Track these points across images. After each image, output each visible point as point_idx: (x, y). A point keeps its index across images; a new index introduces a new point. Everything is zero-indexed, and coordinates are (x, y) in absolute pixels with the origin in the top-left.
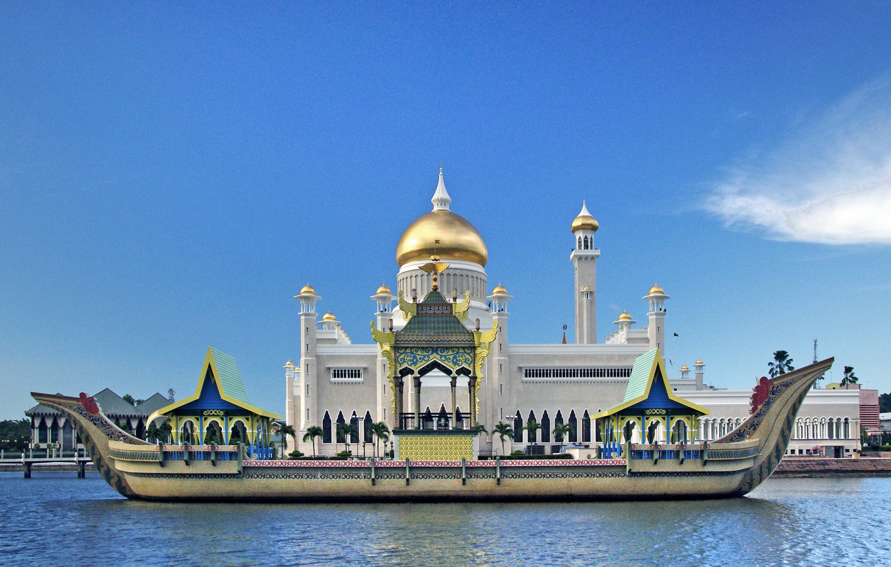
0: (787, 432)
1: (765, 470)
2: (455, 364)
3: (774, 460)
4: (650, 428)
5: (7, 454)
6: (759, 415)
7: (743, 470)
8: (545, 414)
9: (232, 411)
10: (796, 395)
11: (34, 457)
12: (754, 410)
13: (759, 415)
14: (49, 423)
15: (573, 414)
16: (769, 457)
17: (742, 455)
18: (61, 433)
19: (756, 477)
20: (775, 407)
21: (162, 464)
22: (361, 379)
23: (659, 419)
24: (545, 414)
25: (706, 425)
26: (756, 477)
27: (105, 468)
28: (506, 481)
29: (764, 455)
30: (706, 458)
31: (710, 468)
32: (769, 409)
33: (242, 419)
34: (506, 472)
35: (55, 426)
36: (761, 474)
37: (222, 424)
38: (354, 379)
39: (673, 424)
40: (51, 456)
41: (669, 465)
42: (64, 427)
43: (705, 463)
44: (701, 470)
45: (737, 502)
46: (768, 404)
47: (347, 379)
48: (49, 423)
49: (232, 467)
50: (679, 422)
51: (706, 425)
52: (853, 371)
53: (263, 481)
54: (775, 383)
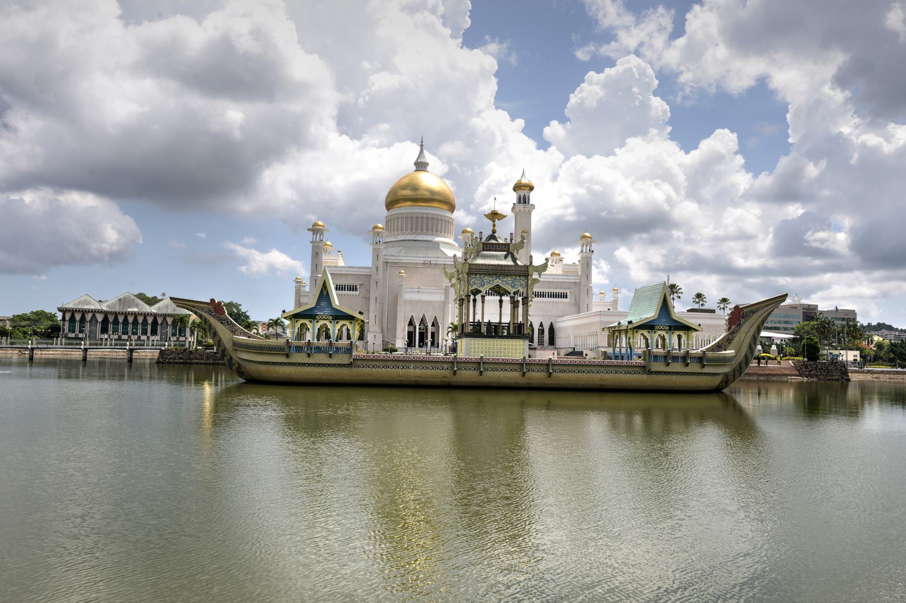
0: (753, 346)
1: (737, 373)
2: (513, 287)
4: (319, 329)
5: (13, 340)
10: (760, 319)
11: (136, 345)
12: (729, 329)
16: (740, 364)
17: (725, 360)
18: (87, 325)
19: (731, 378)
20: (744, 328)
21: (287, 356)
22: (357, 293)
26: (731, 378)
27: (228, 357)
29: (735, 363)
31: (706, 370)
32: (740, 329)
35: (83, 319)
36: (734, 375)
37: (330, 326)
38: (352, 292)
39: (298, 325)
40: (106, 345)
41: (322, 358)
42: (90, 321)
43: (703, 366)
44: (699, 370)
46: (739, 325)
49: (343, 359)
50: (302, 325)
53: (368, 370)
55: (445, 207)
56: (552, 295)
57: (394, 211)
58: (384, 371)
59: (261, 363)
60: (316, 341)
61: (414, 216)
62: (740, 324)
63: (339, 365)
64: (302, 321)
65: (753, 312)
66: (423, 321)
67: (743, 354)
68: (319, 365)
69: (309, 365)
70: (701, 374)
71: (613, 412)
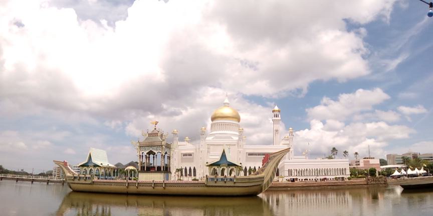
0: (273, 177)
3: (270, 182)
6: (265, 166)
7: (258, 185)
8: (246, 168)
9: (96, 166)
10: (278, 160)
13: (265, 166)
14: (116, 171)
15: (194, 168)
16: (268, 181)
20: (270, 164)
23: (225, 167)
24: (246, 168)
25: (79, 169)
28: (167, 188)
30: (235, 181)
33: (234, 167)
34: (167, 185)
37: (93, 169)
45: (251, 202)
47: (257, 156)
48: (116, 171)
49: (89, 181)
50: (233, 169)
51: (79, 169)
52: (110, 29)
54: (271, 156)
55: (236, 120)
56: (255, 154)
57: (214, 122)
58: (180, 188)
59: (251, 186)
60: (229, 175)
61: (227, 124)
62: (268, 162)
63: (230, 186)
64: (214, 167)
65: (274, 157)
66: (190, 169)
67: (269, 177)
68: (221, 186)
69: (216, 186)
70: (234, 187)
71: (204, 208)
